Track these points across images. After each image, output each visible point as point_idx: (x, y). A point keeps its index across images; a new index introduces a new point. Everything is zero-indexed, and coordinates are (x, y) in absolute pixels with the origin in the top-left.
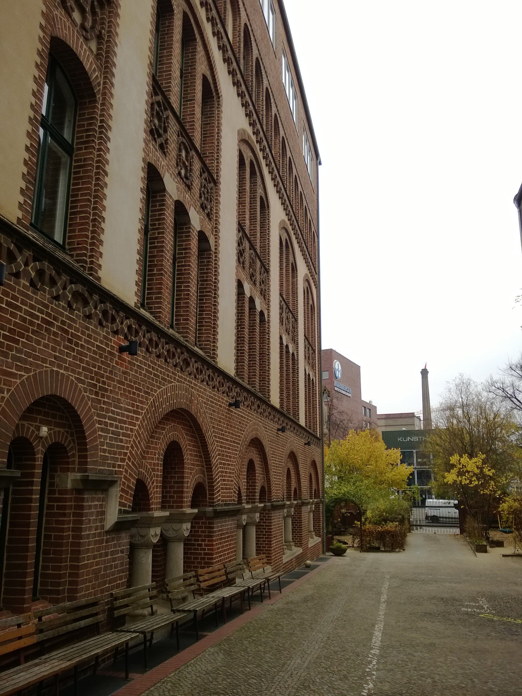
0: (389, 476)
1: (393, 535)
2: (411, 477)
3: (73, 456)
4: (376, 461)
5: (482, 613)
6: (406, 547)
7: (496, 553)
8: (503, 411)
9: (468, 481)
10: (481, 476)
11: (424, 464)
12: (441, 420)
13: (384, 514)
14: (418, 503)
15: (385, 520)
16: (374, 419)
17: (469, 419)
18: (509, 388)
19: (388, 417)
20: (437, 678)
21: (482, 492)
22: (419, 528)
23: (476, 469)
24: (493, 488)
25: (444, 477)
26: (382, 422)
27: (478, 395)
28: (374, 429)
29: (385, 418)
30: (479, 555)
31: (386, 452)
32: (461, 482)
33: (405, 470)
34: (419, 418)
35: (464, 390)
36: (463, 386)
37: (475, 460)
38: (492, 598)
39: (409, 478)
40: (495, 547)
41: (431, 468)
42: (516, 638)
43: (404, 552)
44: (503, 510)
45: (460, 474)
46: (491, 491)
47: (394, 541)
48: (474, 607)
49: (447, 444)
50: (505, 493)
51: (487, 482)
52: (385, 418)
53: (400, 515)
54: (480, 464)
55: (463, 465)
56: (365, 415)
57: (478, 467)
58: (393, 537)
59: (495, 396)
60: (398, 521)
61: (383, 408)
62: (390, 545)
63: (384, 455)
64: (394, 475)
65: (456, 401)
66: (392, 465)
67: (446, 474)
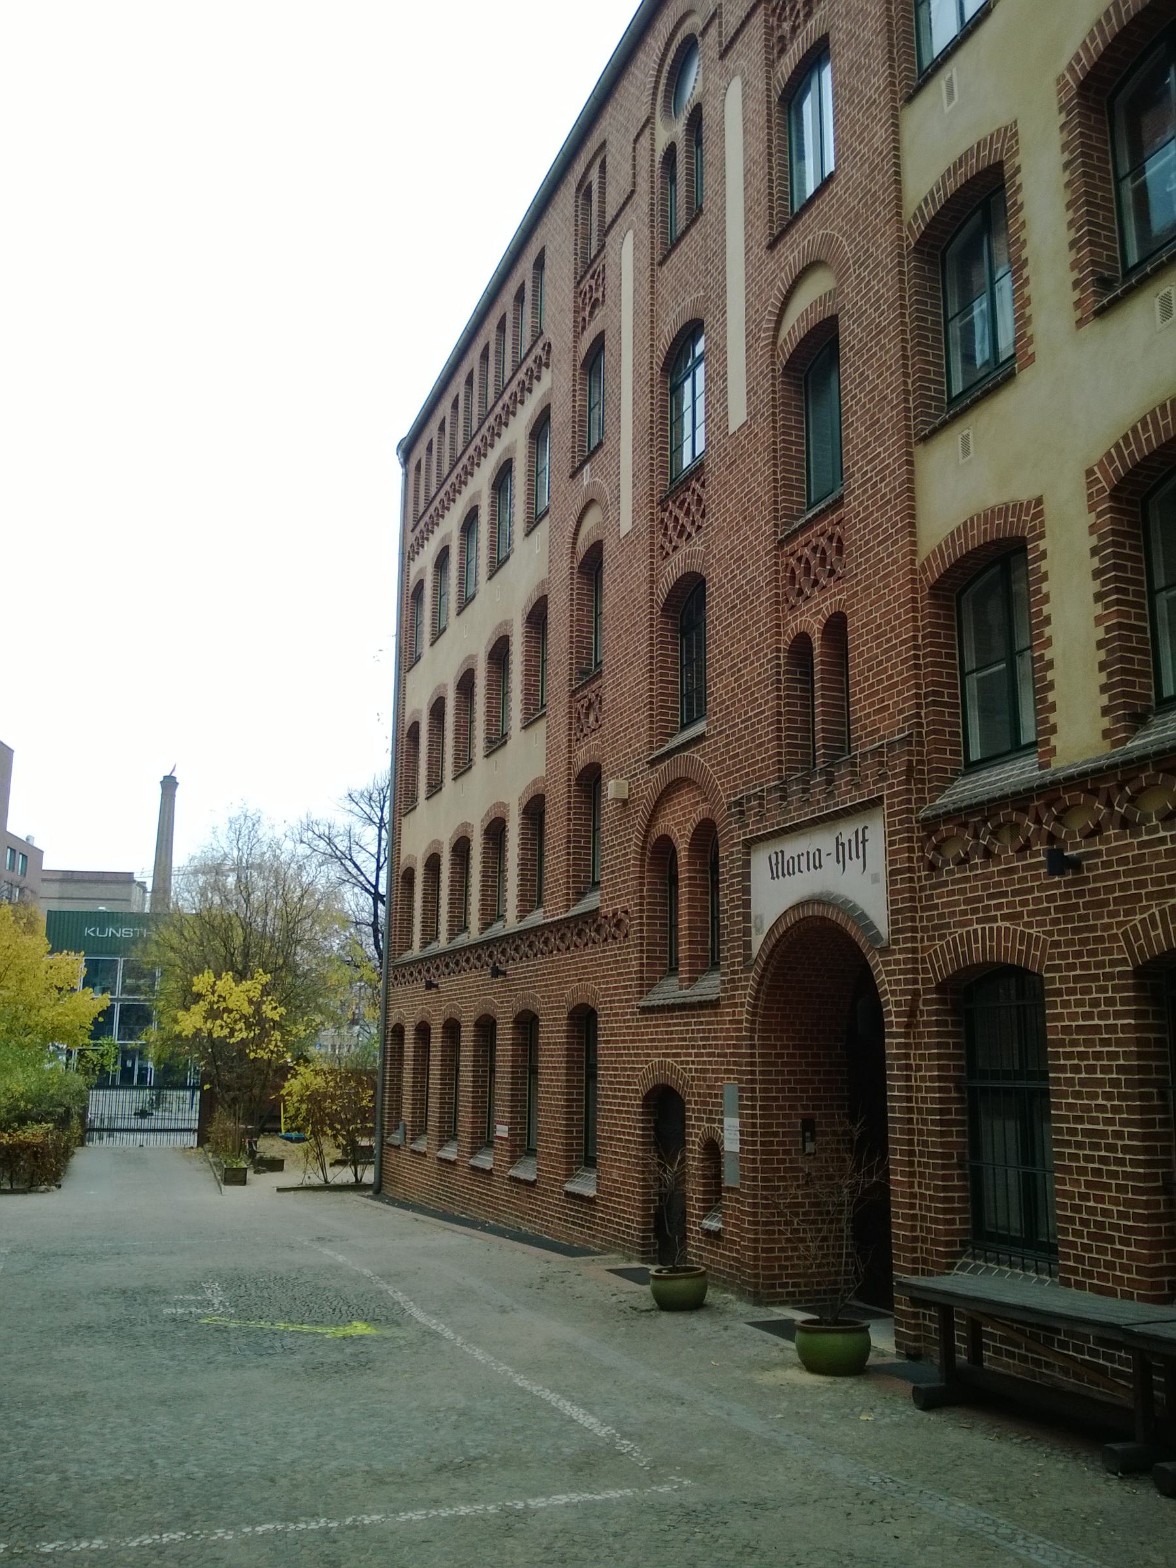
0: (49, 1014)
1: (35, 1154)
2: (101, 1019)
3: (877, 965)
4: (22, 980)
5: (207, 1316)
6: (66, 1182)
7: (263, 1184)
8: (321, 884)
9: (226, 1031)
10: (257, 1020)
11: (135, 990)
12: (186, 895)
13: (22, 1104)
14: (114, 1077)
15: (23, 1119)
16: (30, 881)
17: (249, 895)
18: (341, 838)
19: (69, 878)
20: (73, 1468)
21: (252, 1055)
22: (105, 1134)
23: (246, 1004)
24: (276, 1046)
25: (176, 1021)
26: (54, 889)
27: (275, 845)
28: (26, 905)
29: (62, 881)
30: (230, 1190)
31: (48, 959)
32: (210, 1033)
33: (92, 1002)
34: (142, 885)
35: (245, 832)
36: (245, 827)
37: (247, 984)
38: (233, 1282)
39: (95, 1022)
40: (264, 1172)
41: (149, 1000)
42: (266, 1361)
43: (58, 1191)
44: (289, 1094)
45: (213, 1014)
46: (272, 1052)
47: (38, 1167)
48: (191, 1303)
49: (192, 948)
50: (303, 1059)
51: (265, 1034)
52: (62, 881)
53: (61, 1105)
54: (256, 994)
55: (220, 996)
56: (13, 867)
57: (251, 1002)
58: (36, 1158)
59: (309, 852)
60: (53, 1121)
61: (58, 857)
62: (26, 1176)
63: (43, 966)
64: (60, 1014)
65: (226, 855)
66: (60, 989)
67: (181, 1014)
